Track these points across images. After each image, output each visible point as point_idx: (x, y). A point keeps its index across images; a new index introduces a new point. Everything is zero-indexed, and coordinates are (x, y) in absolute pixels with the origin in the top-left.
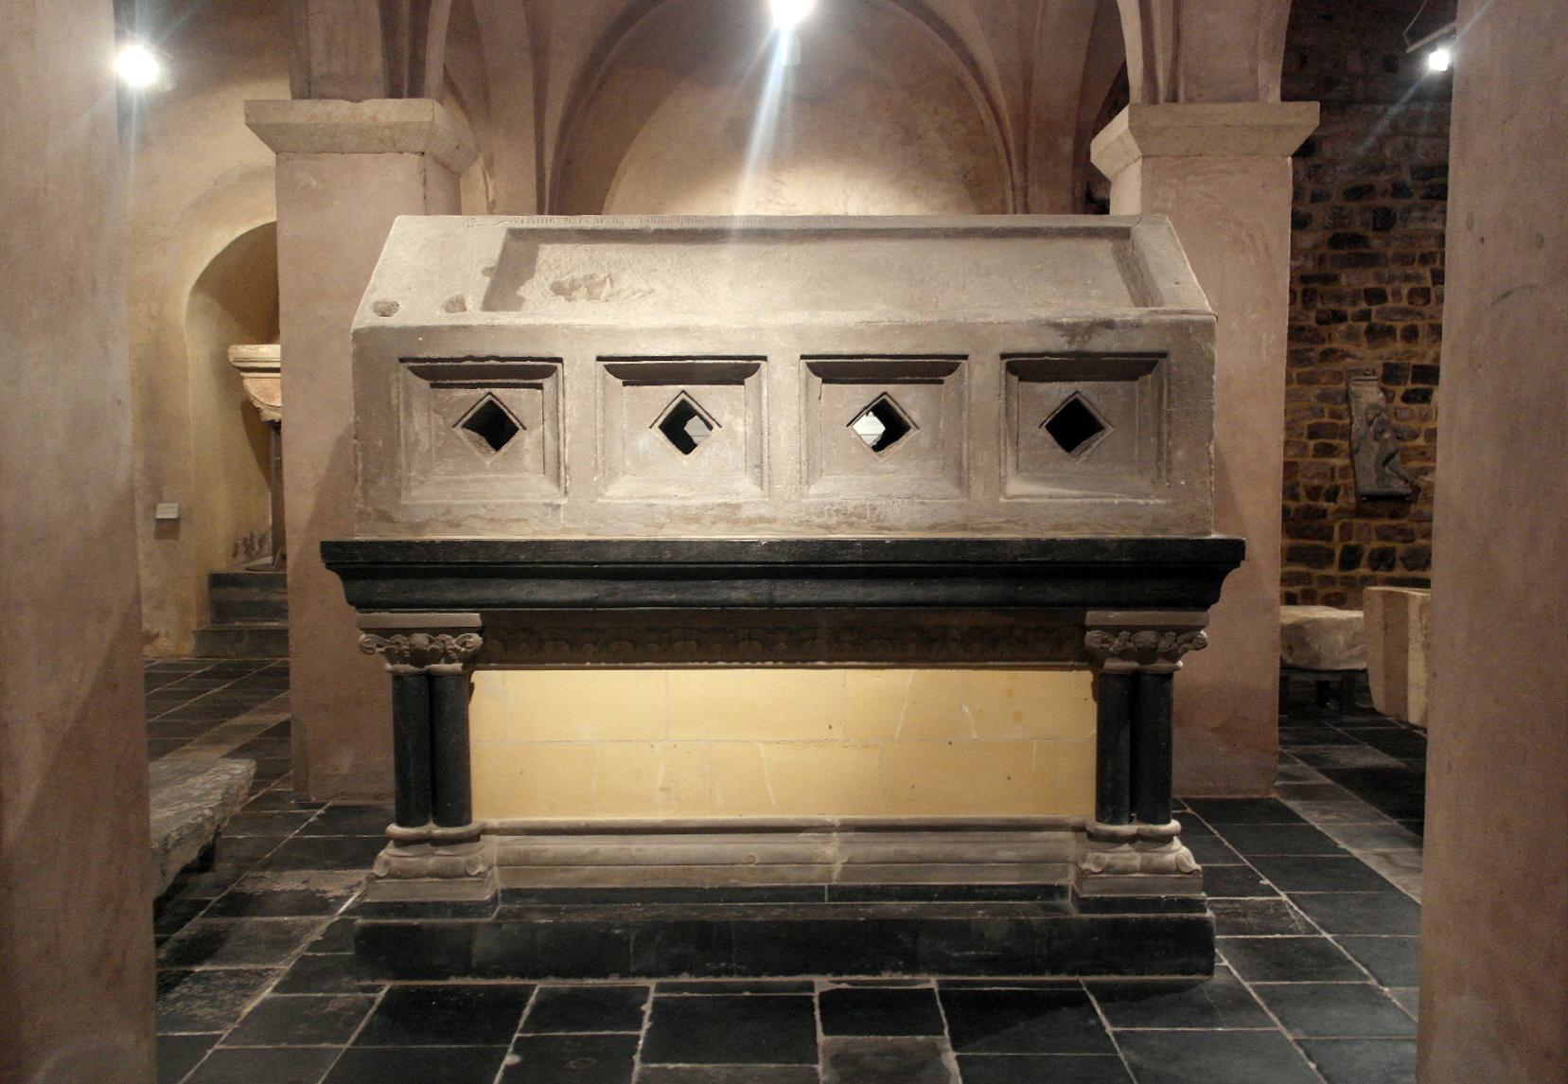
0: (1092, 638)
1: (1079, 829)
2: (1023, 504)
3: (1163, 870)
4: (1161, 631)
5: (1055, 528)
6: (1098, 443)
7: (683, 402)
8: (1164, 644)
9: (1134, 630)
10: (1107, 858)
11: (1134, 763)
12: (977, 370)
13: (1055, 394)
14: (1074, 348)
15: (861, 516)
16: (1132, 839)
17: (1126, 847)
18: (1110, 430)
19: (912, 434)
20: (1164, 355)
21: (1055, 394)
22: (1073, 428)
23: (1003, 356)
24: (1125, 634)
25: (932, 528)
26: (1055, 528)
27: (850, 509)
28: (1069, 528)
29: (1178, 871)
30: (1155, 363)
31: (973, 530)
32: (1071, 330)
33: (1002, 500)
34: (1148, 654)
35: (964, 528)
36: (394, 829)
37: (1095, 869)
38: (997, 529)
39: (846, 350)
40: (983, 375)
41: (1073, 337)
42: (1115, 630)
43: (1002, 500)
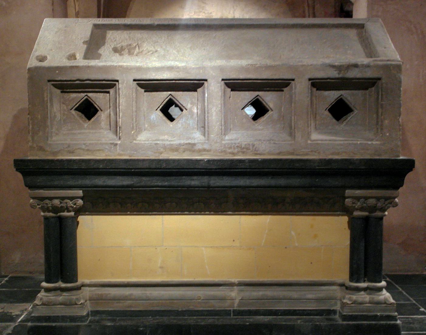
0: (348, 201)
1: (342, 285)
3: (378, 303)
4: (378, 199)
5: (333, 154)
7: (258, 99)
8: (379, 205)
9: (366, 198)
10: (354, 297)
11: (366, 259)
13: (332, 96)
14: (341, 76)
15: (248, 149)
16: (365, 289)
17: (362, 293)
18: (356, 112)
20: (379, 79)
21: (332, 96)
22: (340, 111)
23: (310, 79)
24: (362, 200)
25: (279, 154)
26: (333, 154)
27: (243, 146)
29: (385, 303)
30: (375, 83)
31: (297, 155)
34: (373, 209)
35: (292, 154)
36: (44, 284)
37: (349, 302)
38: (307, 154)
40: (301, 88)
41: (340, 71)
42: (358, 198)
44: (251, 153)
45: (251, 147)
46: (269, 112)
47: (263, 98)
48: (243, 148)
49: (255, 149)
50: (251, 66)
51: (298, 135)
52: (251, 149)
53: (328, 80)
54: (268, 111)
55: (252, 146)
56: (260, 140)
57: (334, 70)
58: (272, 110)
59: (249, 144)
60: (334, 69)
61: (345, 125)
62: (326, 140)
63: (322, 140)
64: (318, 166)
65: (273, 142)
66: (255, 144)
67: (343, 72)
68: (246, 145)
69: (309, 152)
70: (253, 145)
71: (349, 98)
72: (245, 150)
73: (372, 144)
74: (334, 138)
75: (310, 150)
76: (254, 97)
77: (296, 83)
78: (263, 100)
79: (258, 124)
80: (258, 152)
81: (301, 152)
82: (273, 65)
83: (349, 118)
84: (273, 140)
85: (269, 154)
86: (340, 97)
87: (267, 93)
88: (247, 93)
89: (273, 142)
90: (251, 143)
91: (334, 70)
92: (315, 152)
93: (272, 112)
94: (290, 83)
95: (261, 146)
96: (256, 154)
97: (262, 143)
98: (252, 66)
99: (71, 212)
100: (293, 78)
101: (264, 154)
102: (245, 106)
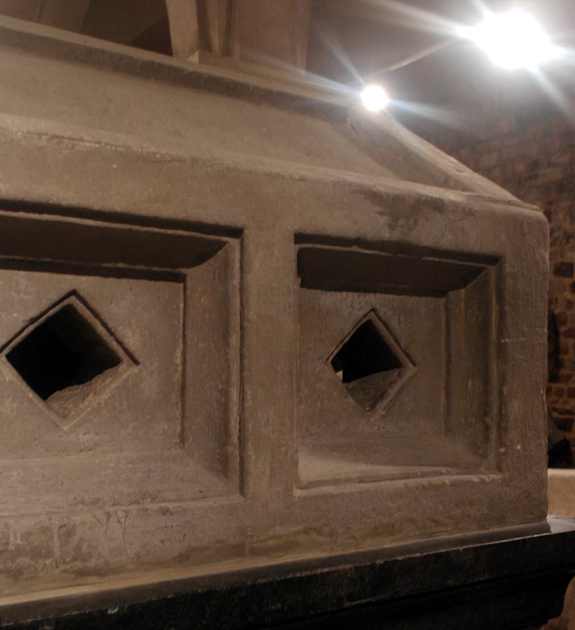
2: (325, 497)
5: (376, 532)
6: (106, 388)
7: (70, 309)
12: (257, 259)
13: (347, 309)
14: (396, 236)
15: (39, 553)
18: (410, 370)
19: (125, 372)
20: (495, 260)
21: (347, 309)
23: (299, 237)
25: (183, 559)
26: (376, 532)
27: (15, 541)
28: (389, 530)
30: (477, 272)
31: (255, 553)
32: (394, 206)
33: (298, 493)
35: (238, 551)
38: (290, 546)
39: (116, 202)
40: (268, 266)
41: (395, 217)
43: (298, 493)
44: (57, 571)
45: (56, 543)
46: (121, 368)
47: (94, 305)
48: (19, 551)
49: (78, 548)
50: (55, 141)
51: (259, 467)
52: (57, 551)
53: (355, 248)
54: (114, 361)
55: (60, 538)
56: (95, 502)
57: (376, 213)
58: (136, 362)
59: (45, 530)
60: (379, 209)
61: (383, 417)
62: (348, 480)
63: (335, 482)
64: (350, 597)
65: (155, 506)
66: (74, 526)
67: (401, 222)
68: (28, 535)
69: (299, 532)
70: (68, 533)
71: (394, 323)
72: (24, 560)
73: (483, 481)
74: (362, 468)
75: (300, 527)
76: (54, 296)
77: (251, 247)
78: (96, 315)
79: (72, 424)
80: (92, 563)
81: (272, 538)
82: (155, 154)
83: (393, 391)
84: (153, 499)
85: (141, 564)
86: (66, 302)
87: (111, 282)
88: (21, 277)
89: (155, 506)
90: (56, 522)
91: (376, 213)
92: (319, 532)
93: (135, 369)
94: (221, 245)
95: (105, 532)
96: (82, 574)
97: (108, 515)
98: (58, 143)
99: (145, 62)
100: (239, 224)
101: (118, 570)
102: (10, 338)
